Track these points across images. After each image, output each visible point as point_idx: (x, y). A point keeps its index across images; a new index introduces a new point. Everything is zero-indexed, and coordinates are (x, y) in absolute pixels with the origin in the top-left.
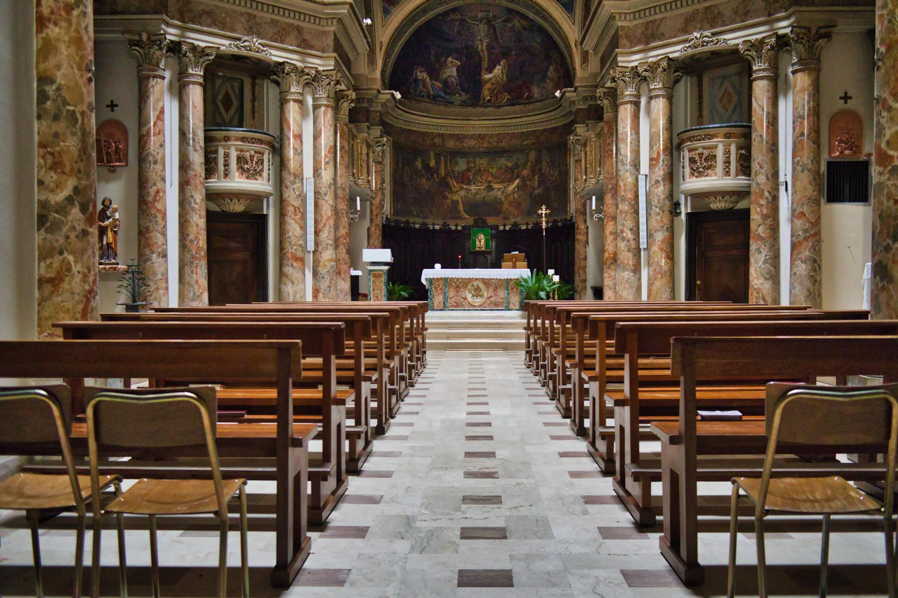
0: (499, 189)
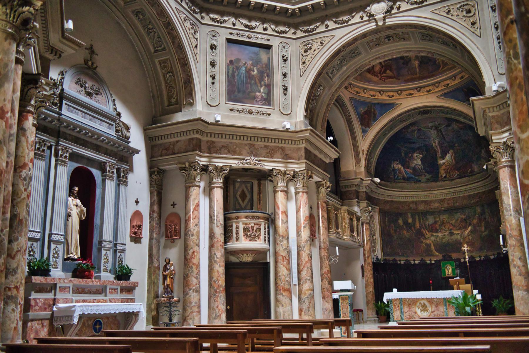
0: (458, 234)
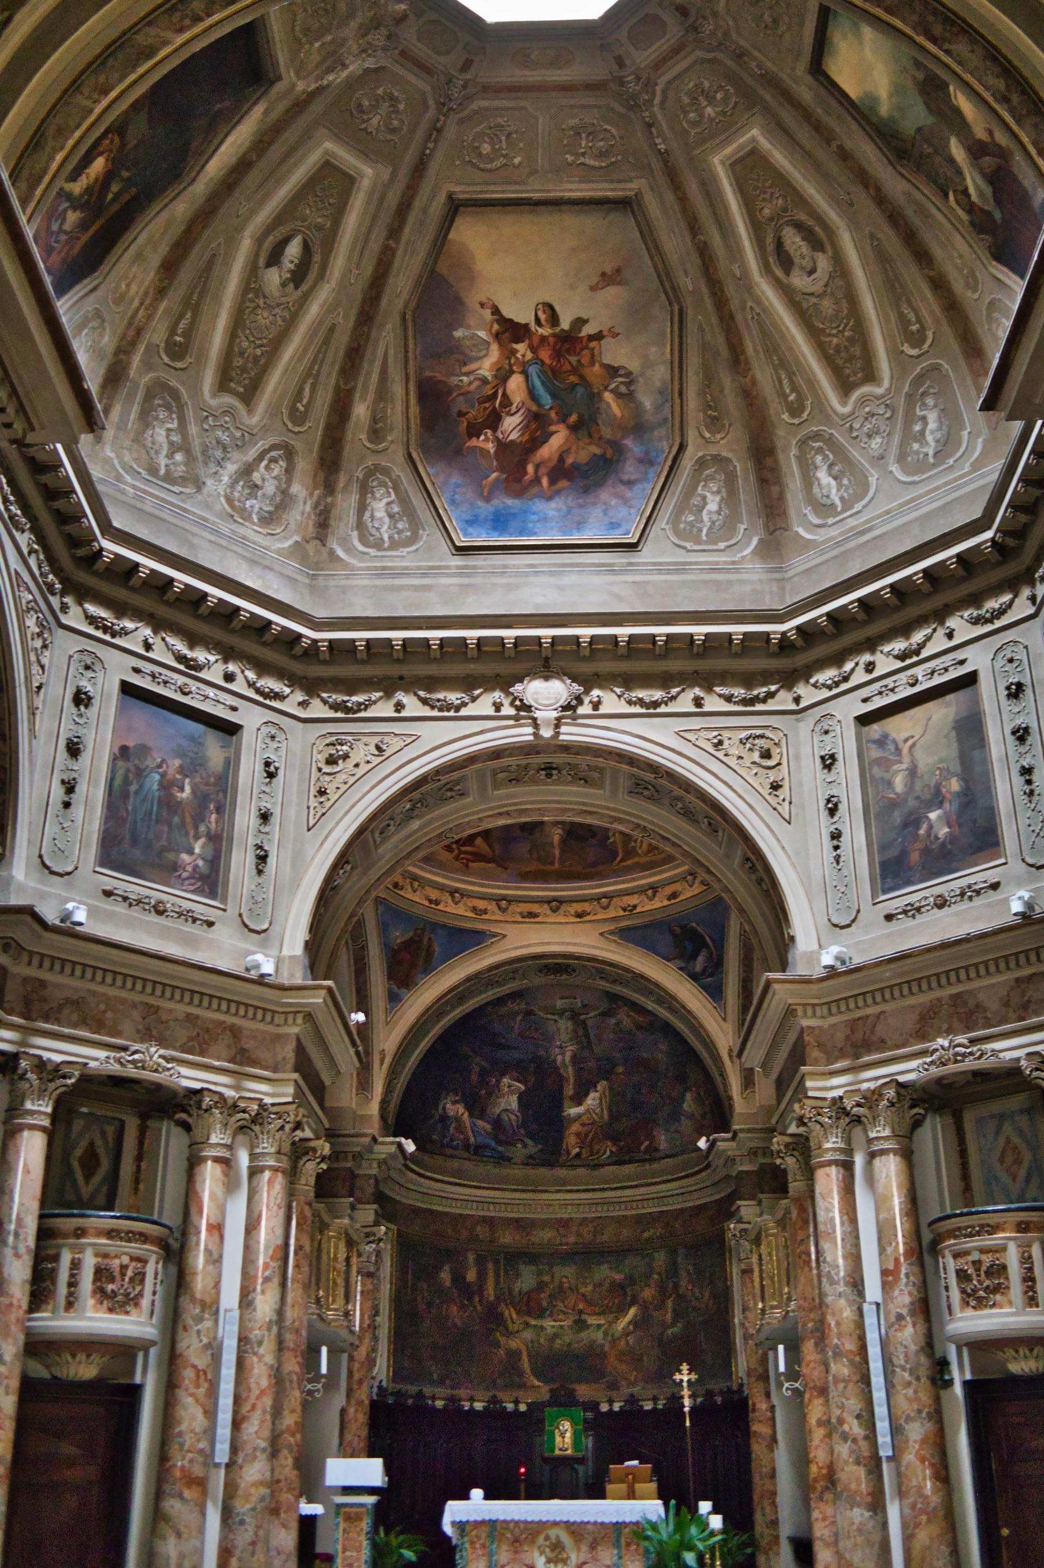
0: (599, 1326)
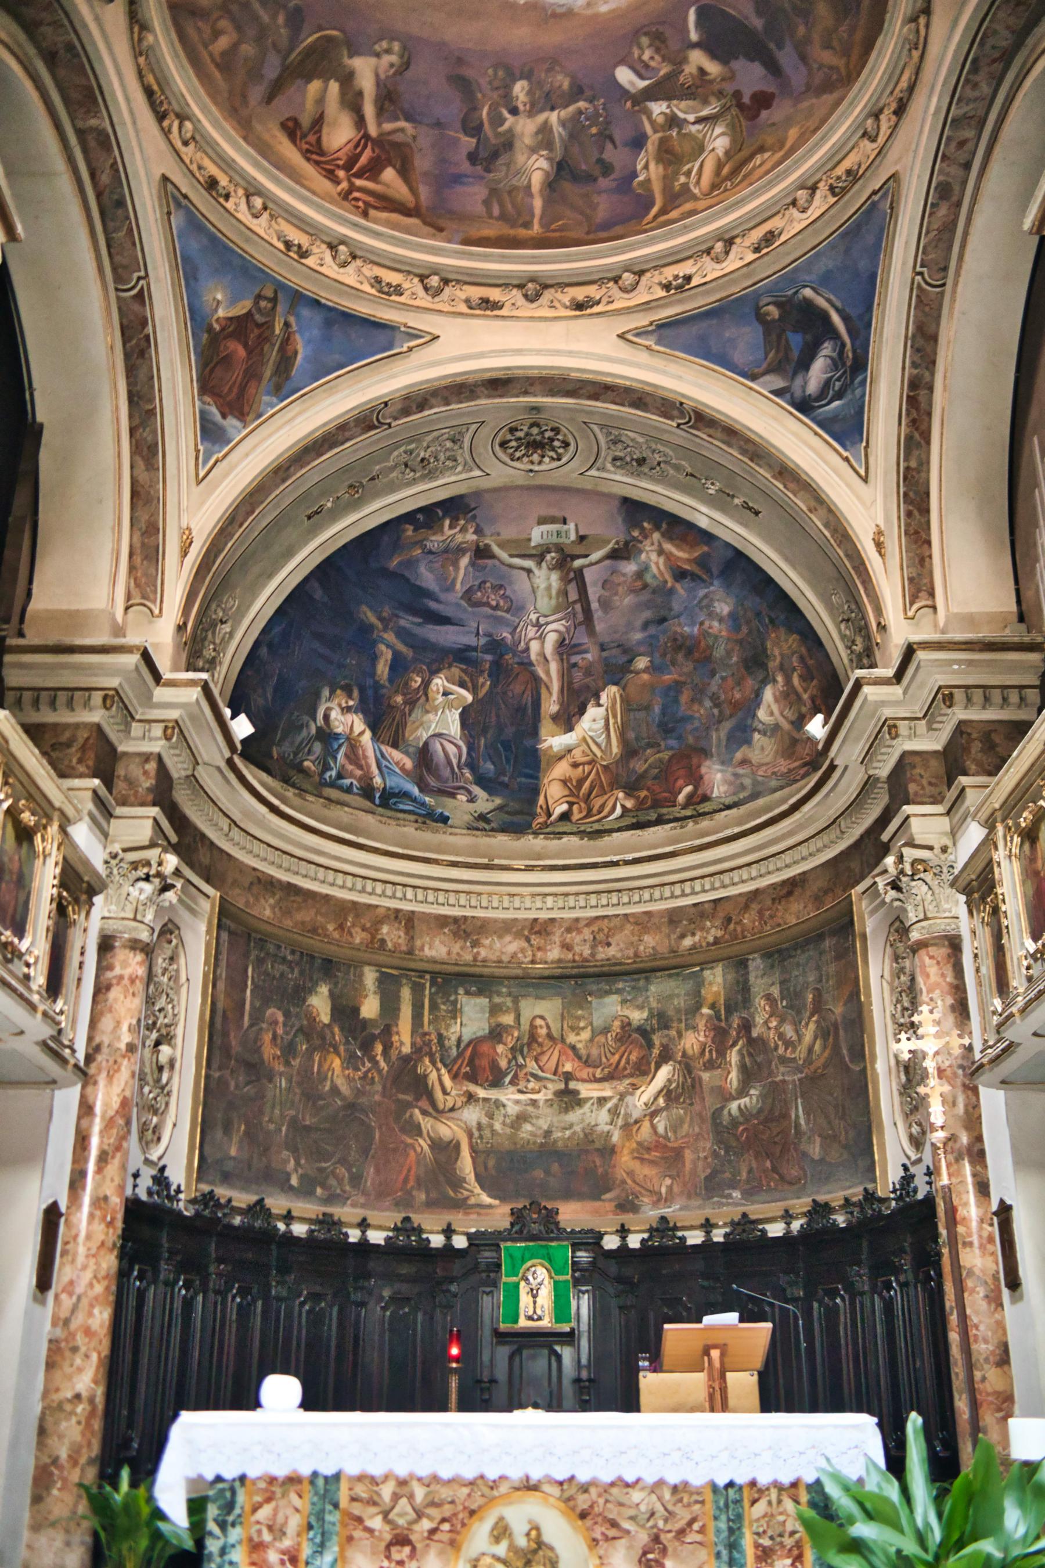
0: (602, 1101)
